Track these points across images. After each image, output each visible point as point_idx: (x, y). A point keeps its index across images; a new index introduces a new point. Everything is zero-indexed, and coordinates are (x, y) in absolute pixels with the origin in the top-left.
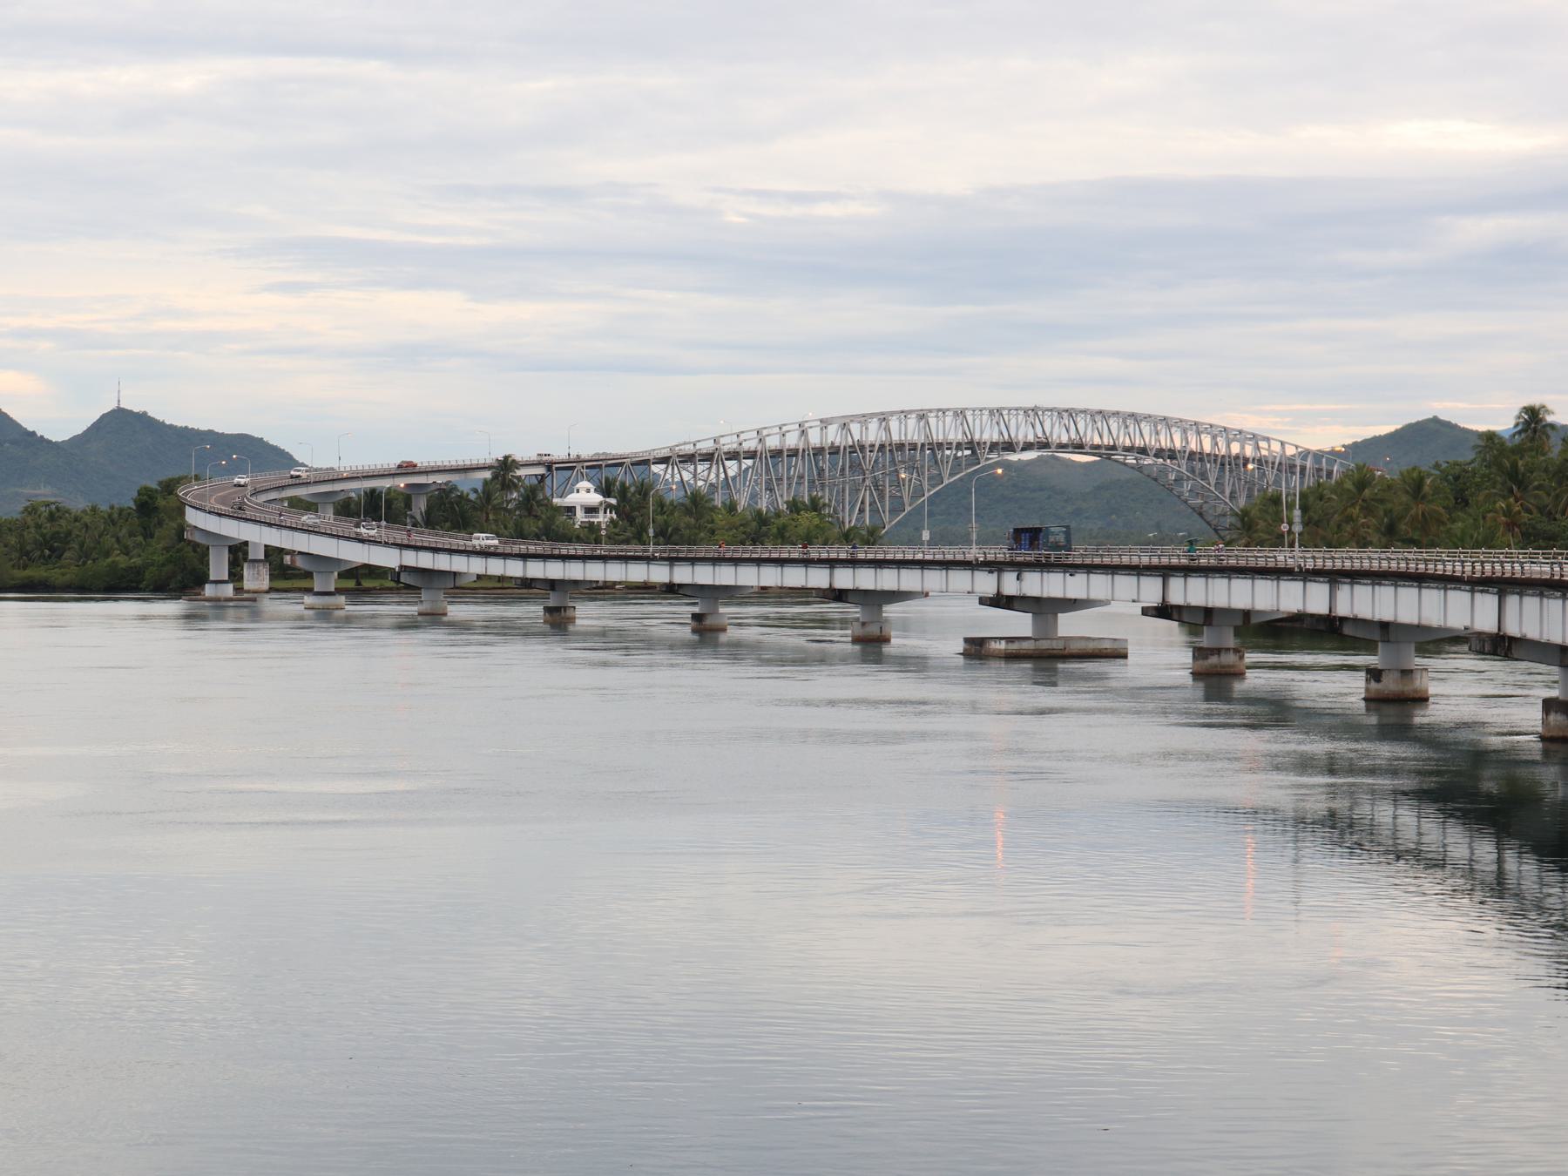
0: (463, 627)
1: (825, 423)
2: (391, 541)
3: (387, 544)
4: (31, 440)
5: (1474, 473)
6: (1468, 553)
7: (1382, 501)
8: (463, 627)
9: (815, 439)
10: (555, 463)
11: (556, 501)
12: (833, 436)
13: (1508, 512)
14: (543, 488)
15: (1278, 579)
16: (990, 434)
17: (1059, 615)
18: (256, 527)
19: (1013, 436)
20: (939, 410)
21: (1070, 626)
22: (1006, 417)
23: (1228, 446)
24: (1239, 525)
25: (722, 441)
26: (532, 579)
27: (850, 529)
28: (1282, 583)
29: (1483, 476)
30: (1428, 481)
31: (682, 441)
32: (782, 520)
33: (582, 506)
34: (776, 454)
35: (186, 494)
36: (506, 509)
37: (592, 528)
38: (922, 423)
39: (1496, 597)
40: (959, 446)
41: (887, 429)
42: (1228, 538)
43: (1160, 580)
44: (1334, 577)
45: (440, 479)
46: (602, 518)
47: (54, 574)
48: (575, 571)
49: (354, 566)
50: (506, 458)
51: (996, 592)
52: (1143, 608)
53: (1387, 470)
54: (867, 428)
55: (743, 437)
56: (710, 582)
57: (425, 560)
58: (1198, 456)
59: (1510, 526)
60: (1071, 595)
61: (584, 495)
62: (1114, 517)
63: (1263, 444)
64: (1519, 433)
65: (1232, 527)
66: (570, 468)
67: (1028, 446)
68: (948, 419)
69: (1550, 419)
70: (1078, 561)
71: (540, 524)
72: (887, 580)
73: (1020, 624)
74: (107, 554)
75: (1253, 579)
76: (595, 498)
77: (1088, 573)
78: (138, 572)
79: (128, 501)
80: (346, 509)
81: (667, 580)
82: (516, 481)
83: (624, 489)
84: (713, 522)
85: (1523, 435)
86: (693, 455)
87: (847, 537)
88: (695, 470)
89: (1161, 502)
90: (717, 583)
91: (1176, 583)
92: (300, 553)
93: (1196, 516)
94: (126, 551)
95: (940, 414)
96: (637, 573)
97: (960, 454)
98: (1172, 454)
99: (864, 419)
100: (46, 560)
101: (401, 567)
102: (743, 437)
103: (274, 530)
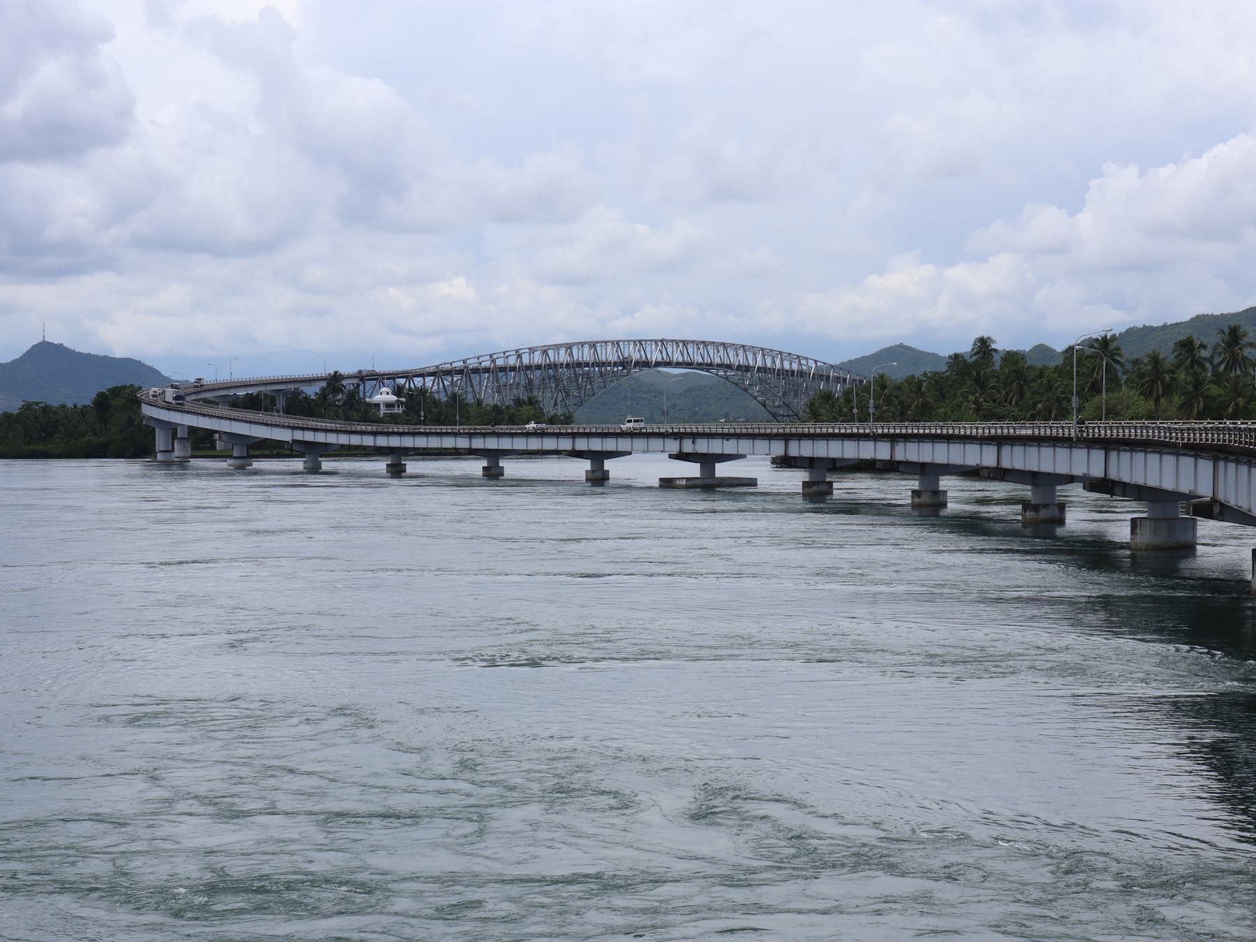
1: (532, 350)
2: (287, 424)
3: (283, 427)
5: (948, 378)
9: (526, 360)
11: (367, 400)
12: (538, 359)
13: (976, 402)
14: (358, 392)
15: (858, 440)
17: (717, 465)
18: (194, 417)
19: (649, 358)
20: (603, 342)
21: (723, 470)
25: (468, 362)
26: (380, 447)
28: (936, 445)
29: (954, 380)
30: (925, 384)
31: (443, 362)
32: (512, 411)
33: (384, 403)
34: (529, 368)
35: (142, 396)
38: (592, 351)
39: (996, 447)
40: (615, 364)
41: (571, 354)
43: (783, 443)
44: (893, 439)
45: (292, 387)
46: (398, 410)
48: (408, 442)
49: (255, 441)
50: (336, 373)
51: (783, 454)
52: (773, 458)
54: (558, 354)
55: (481, 359)
57: (309, 436)
59: (977, 410)
60: (727, 452)
61: (384, 396)
62: (697, 409)
63: (803, 362)
64: (975, 354)
66: (378, 378)
67: (678, 365)
68: (609, 347)
69: (993, 346)
71: (360, 415)
72: (610, 445)
73: (692, 470)
74: (83, 435)
75: (843, 440)
76: (393, 398)
77: (738, 438)
80: (235, 403)
81: (468, 447)
84: (468, 412)
85: (977, 357)
86: (451, 371)
88: (452, 380)
90: (500, 448)
92: (224, 432)
94: (95, 433)
95: (603, 344)
97: (616, 369)
98: (747, 369)
99: (557, 347)
101: (293, 440)
102: (481, 359)
103: (207, 419)
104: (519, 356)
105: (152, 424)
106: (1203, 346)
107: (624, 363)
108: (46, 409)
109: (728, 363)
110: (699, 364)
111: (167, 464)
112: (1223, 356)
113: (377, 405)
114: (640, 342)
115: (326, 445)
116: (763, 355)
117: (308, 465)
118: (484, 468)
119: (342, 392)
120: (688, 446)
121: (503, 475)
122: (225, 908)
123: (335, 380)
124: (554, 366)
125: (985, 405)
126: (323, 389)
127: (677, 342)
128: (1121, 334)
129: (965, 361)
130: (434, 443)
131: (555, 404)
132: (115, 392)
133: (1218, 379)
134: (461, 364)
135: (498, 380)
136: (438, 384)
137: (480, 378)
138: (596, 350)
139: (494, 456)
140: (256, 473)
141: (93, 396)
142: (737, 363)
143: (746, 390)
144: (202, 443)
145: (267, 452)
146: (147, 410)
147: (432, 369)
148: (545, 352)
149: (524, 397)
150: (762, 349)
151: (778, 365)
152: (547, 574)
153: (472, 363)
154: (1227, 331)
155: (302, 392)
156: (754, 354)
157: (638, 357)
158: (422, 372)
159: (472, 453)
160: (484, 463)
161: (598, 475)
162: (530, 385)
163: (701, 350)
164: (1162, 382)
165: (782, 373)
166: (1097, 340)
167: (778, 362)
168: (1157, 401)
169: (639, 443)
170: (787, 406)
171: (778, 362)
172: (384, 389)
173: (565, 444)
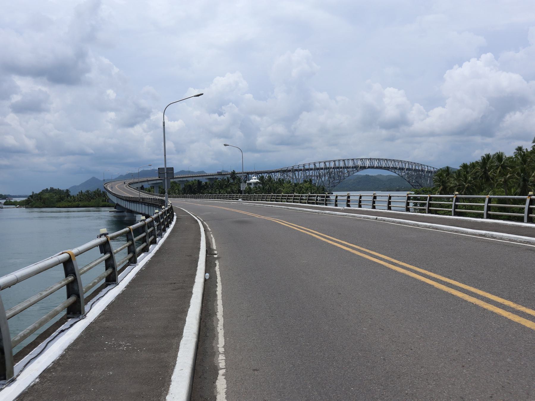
0: (32, 382)
6: (425, 199)
8: (32, 382)
10: (249, 172)
12: (322, 165)
20: (347, 159)
22: (364, 161)
41: (335, 164)
58: (408, 169)
82: (237, 177)
99: (330, 162)
104: (315, 165)
109: (396, 167)
116: (408, 164)
134: (286, 169)
137: (309, 173)
138: (345, 162)
142: (399, 167)
153: (296, 168)
156: (405, 164)
165: (415, 170)
167: (414, 167)
170: (417, 182)
171: (414, 167)
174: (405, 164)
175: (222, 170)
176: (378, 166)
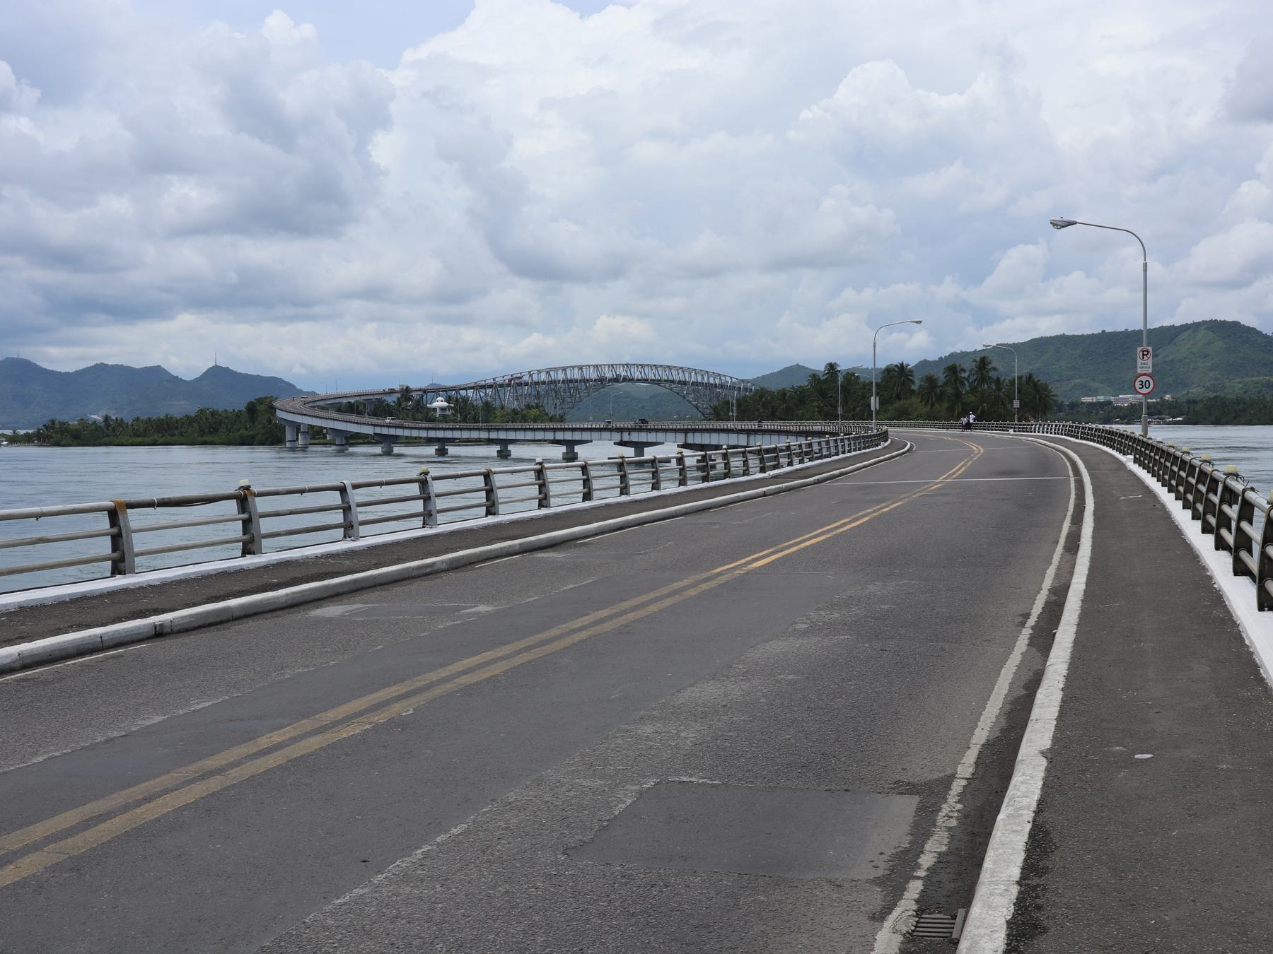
1: (539, 372)
3: (368, 424)
4: (176, 380)
7: (770, 403)
9: (535, 378)
11: (428, 405)
12: (543, 377)
14: (422, 401)
16: (609, 375)
17: (575, 447)
20: (587, 366)
23: (708, 379)
24: (713, 412)
27: (552, 416)
34: (537, 383)
36: (407, 409)
37: (444, 416)
41: (566, 374)
42: (709, 418)
43: (553, 433)
46: (448, 413)
47: (216, 439)
48: (449, 434)
53: (775, 387)
55: (505, 378)
56: (505, 438)
59: (820, 412)
62: (659, 409)
64: (826, 374)
65: (710, 414)
66: (436, 391)
68: (592, 369)
69: (839, 369)
70: (652, 427)
72: (577, 436)
74: (239, 430)
78: (253, 437)
79: (243, 408)
80: (340, 409)
83: (457, 400)
86: (484, 386)
87: (551, 420)
89: (679, 402)
91: (690, 436)
93: (694, 408)
96: (475, 435)
98: (685, 383)
99: (556, 369)
100: (211, 433)
103: (318, 419)
104: (531, 376)
105: (283, 423)
106: (964, 370)
107: (601, 380)
108: (214, 413)
110: (652, 380)
111: (293, 450)
112: (975, 377)
113: (435, 409)
114: (612, 365)
115: (396, 437)
116: (696, 374)
117: (385, 449)
118: (498, 451)
119: (412, 400)
120: (626, 437)
121: (510, 455)
122: (895, 914)
123: (406, 392)
124: (554, 382)
125: (825, 408)
126: (398, 399)
127: (637, 365)
128: (945, 357)
129: (819, 379)
130: (465, 435)
131: (555, 408)
132: (260, 401)
133: (973, 390)
135: (516, 392)
136: (476, 395)
138: (582, 371)
139: (505, 443)
140: (352, 455)
141: (245, 405)
143: (684, 397)
144: (317, 436)
145: (361, 441)
146: (279, 414)
147: (472, 385)
148: (548, 373)
149: (533, 402)
150: (695, 370)
151: (706, 380)
152: (366, 512)
153: (499, 381)
154: (978, 359)
155: (385, 400)
157: (611, 376)
158: (465, 386)
159: (490, 442)
160: (498, 448)
161: (571, 455)
162: (538, 395)
163: (654, 370)
164: (935, 394)
165: (708, 386)
166: (897, 366)
167: (706, 378)
168: (932, 405)
169: (595, 435)
171: (706, 378)
172: (439, 398)
173: (549, 436)
174: (690, 373)
175: (213, 364)
176: (640, 377)
